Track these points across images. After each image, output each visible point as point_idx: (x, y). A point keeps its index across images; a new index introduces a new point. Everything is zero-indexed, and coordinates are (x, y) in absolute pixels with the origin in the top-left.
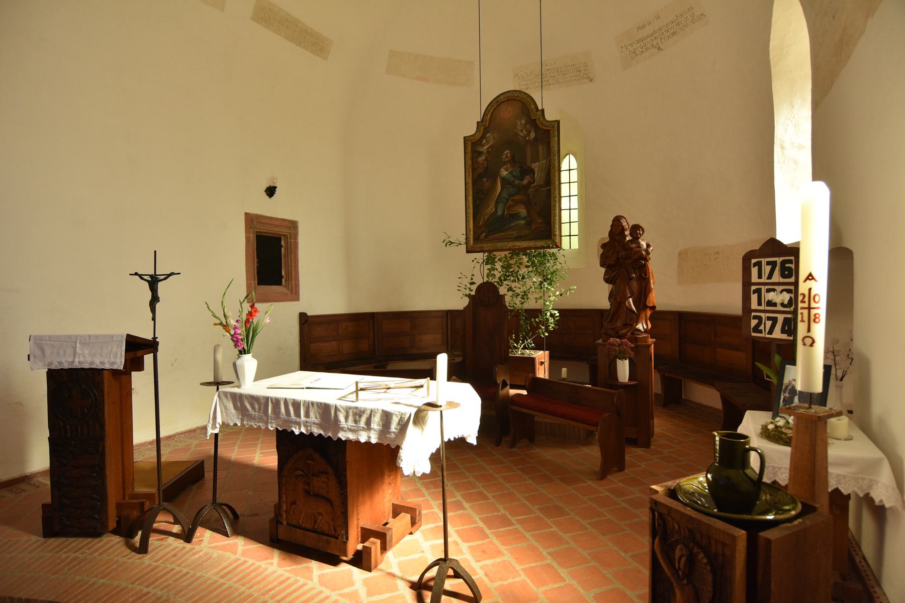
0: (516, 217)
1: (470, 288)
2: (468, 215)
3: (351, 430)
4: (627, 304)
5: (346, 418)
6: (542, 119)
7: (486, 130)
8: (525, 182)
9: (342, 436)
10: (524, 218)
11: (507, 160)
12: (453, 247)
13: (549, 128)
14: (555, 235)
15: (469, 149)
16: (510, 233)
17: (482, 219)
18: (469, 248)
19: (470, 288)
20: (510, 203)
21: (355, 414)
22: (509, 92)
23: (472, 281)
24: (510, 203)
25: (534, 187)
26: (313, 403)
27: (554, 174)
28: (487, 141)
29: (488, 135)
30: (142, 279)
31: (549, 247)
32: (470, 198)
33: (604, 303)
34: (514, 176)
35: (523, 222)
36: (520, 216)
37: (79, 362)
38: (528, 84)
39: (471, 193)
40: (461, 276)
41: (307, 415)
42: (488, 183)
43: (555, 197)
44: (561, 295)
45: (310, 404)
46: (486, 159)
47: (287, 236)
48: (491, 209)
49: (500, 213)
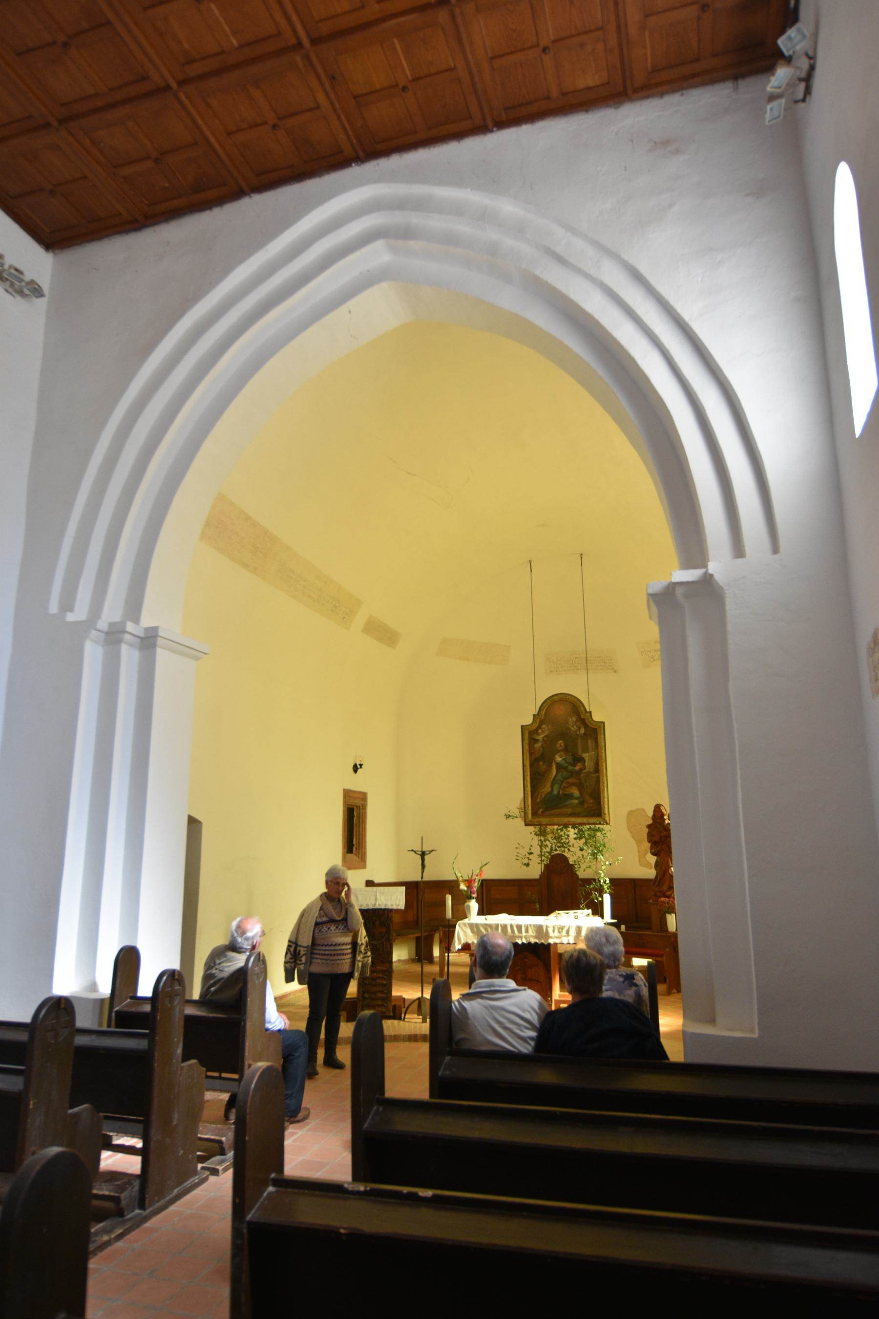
0: (570, 796)
1: (528, 858)
2: (526, 793)
3: (556, 937)
4: (670, 872)
5: (554, 931)
6: (590, 719)
7: (542, 722)
8: (577, 768)
9: (551, 941)
10: (577, 798)
11: (560, 748)
12: (510, 820)
13: (596, 727)
14: (605, 814)
15: (527, 736)
16: (565, 810)
17: (539, 797)
18: (528, 822)
19: (528, 858)
20: (564, 784)
21: (559, 928)
22: (561, 694)
23: (530, 851)
24: (564, 784)
25: (585, 773)
26: (530, 925)
27: (602, 764)
28: (542, 731)
29: (543, 726)
30: (416, 853)
31: (600, 824)
32: (528, 778)
33: (650, 873)
34: (567, 763)
35: (576, 801)
36: (574, 796)
37: (379, 905)
38: (557, 667)
39: (529, 773)
40: (518, 846)
41: (527, 931)
42: (544, 767)
43: (604, 783)
44: (610, 864)
45: (529, 926)
46: (542, 746)
47: (359, 807)
48: (547, 788)
49: (555, 792)
